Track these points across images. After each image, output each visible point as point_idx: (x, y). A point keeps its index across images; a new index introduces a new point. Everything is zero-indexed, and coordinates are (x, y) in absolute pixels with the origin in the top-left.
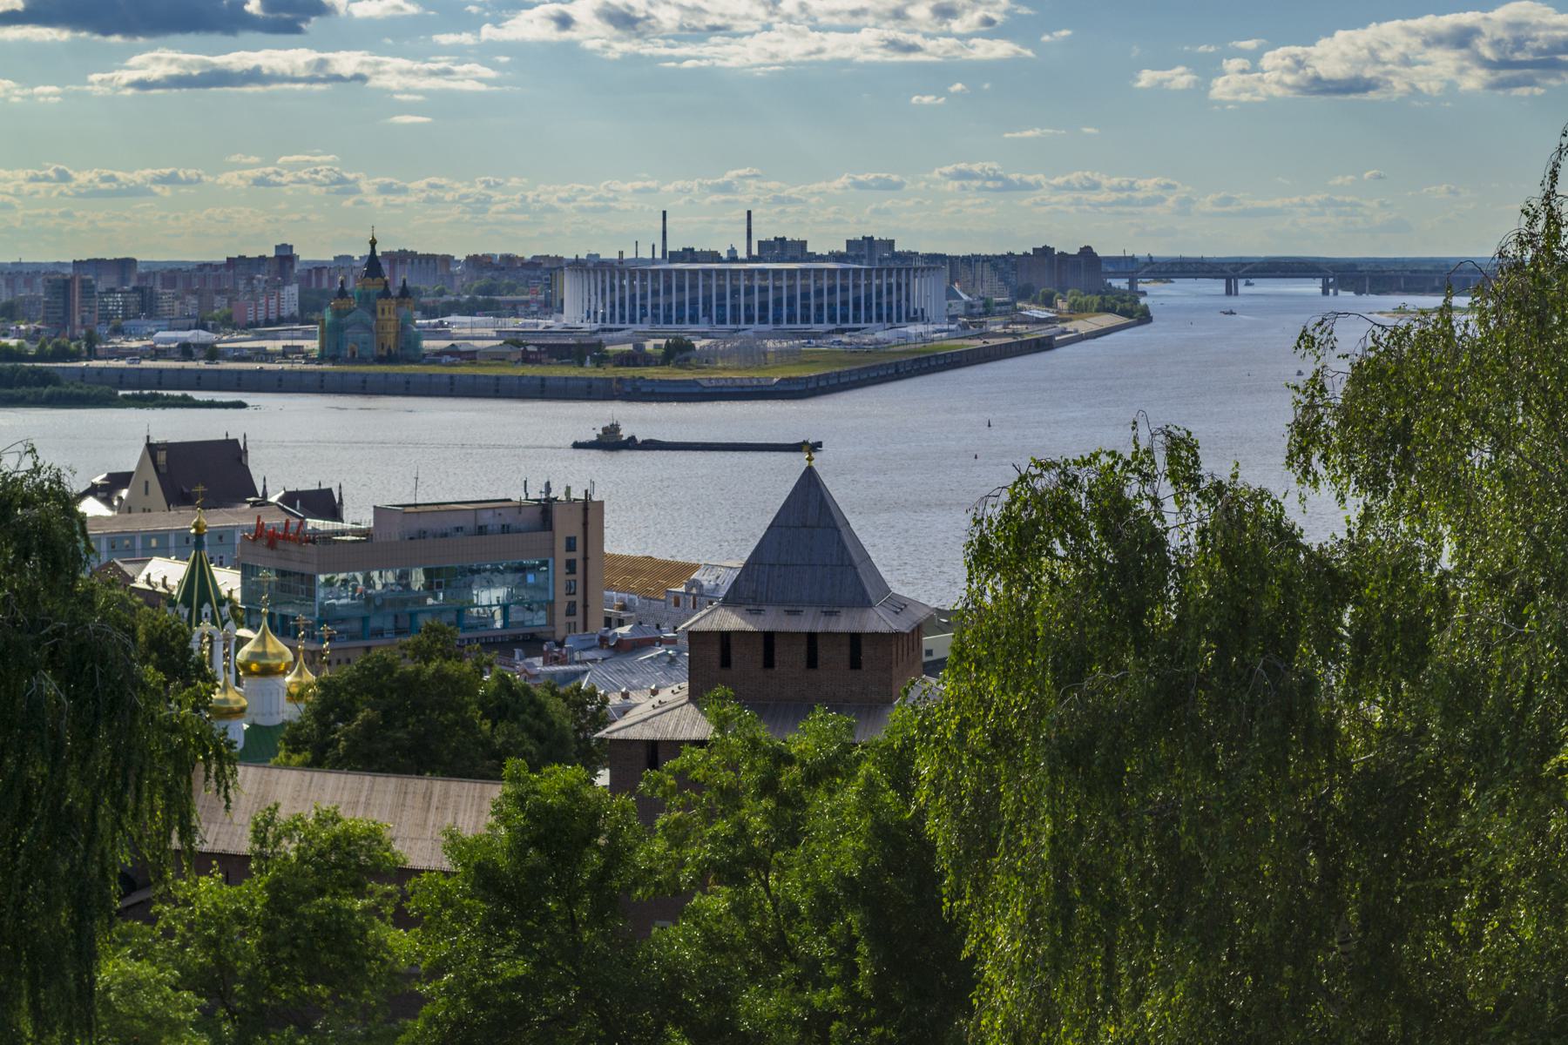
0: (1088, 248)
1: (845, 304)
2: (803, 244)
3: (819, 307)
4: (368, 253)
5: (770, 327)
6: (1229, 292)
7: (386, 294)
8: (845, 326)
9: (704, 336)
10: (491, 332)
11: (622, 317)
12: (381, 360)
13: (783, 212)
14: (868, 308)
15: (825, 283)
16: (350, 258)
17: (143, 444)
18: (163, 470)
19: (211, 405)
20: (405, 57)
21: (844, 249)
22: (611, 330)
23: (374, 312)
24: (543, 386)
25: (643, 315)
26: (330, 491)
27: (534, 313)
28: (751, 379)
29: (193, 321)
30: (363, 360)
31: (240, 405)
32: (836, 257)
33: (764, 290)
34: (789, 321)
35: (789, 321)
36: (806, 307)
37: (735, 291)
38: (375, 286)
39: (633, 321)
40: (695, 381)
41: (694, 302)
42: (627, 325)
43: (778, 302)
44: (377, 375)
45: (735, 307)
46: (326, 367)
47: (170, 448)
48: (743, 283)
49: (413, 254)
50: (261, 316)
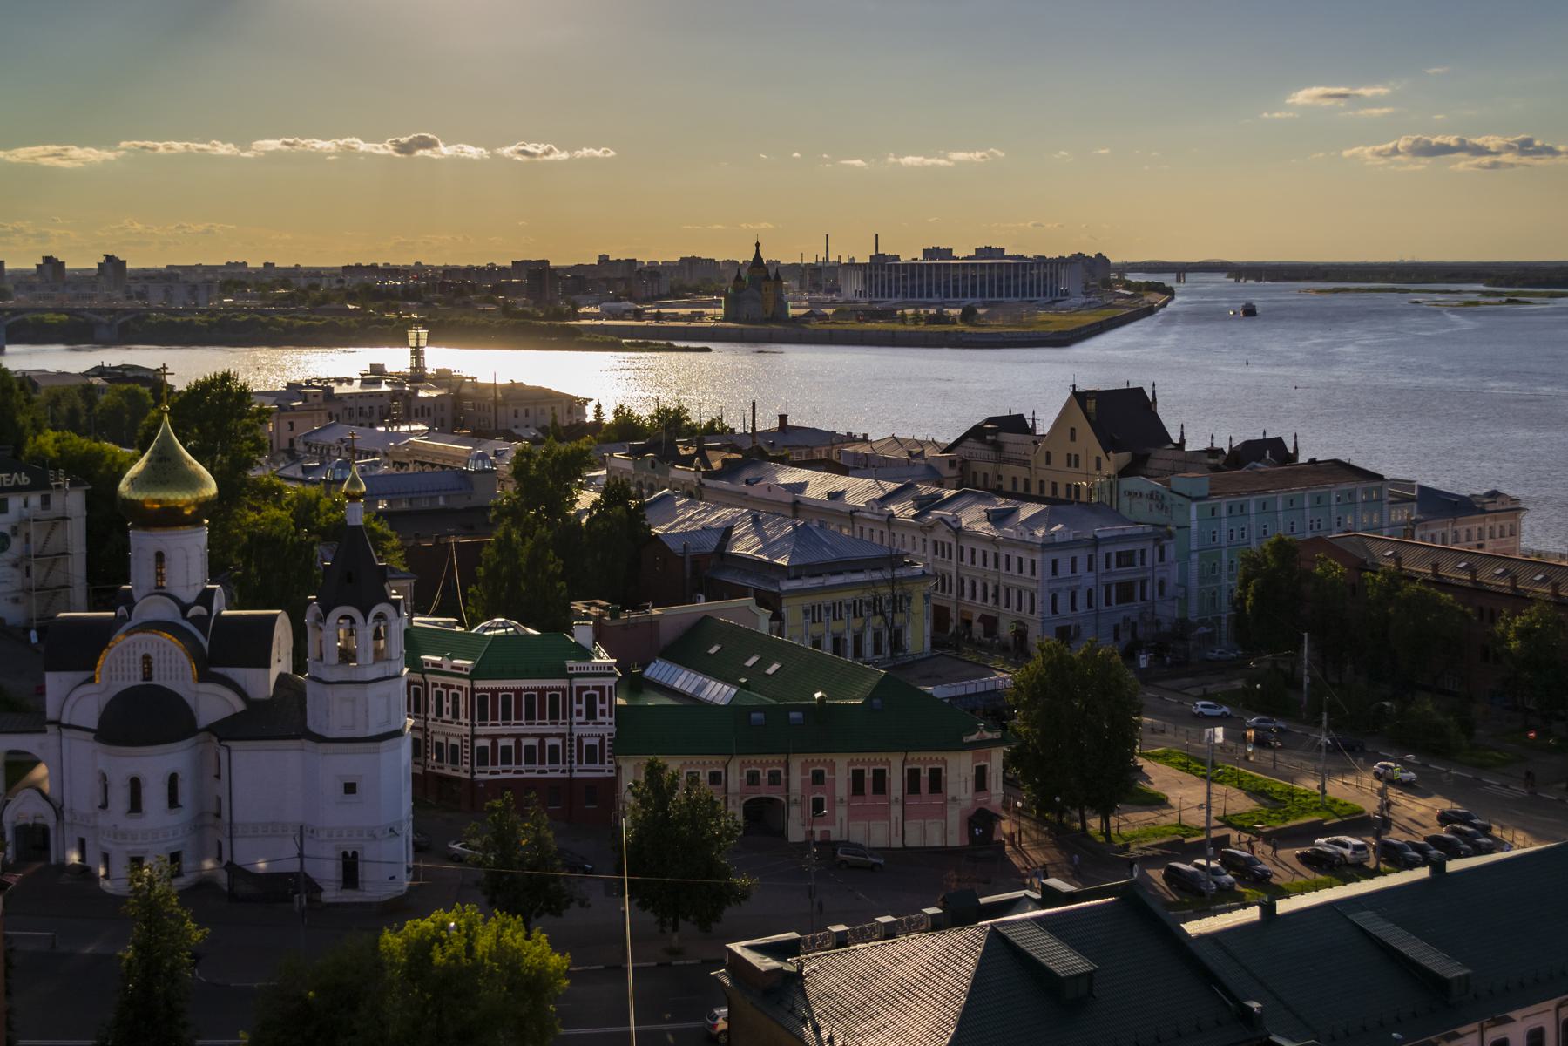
9: (984, 306)
14: (890, 288)
17: (1069, 393)
18: (1093, 418)
19: (687, 350)
25: (897, 292)
31: (708, 350)
32: (969, 258)
33: (974, 277)
36: (1000, 288)
39: (890, 296)
48: (969, 272)
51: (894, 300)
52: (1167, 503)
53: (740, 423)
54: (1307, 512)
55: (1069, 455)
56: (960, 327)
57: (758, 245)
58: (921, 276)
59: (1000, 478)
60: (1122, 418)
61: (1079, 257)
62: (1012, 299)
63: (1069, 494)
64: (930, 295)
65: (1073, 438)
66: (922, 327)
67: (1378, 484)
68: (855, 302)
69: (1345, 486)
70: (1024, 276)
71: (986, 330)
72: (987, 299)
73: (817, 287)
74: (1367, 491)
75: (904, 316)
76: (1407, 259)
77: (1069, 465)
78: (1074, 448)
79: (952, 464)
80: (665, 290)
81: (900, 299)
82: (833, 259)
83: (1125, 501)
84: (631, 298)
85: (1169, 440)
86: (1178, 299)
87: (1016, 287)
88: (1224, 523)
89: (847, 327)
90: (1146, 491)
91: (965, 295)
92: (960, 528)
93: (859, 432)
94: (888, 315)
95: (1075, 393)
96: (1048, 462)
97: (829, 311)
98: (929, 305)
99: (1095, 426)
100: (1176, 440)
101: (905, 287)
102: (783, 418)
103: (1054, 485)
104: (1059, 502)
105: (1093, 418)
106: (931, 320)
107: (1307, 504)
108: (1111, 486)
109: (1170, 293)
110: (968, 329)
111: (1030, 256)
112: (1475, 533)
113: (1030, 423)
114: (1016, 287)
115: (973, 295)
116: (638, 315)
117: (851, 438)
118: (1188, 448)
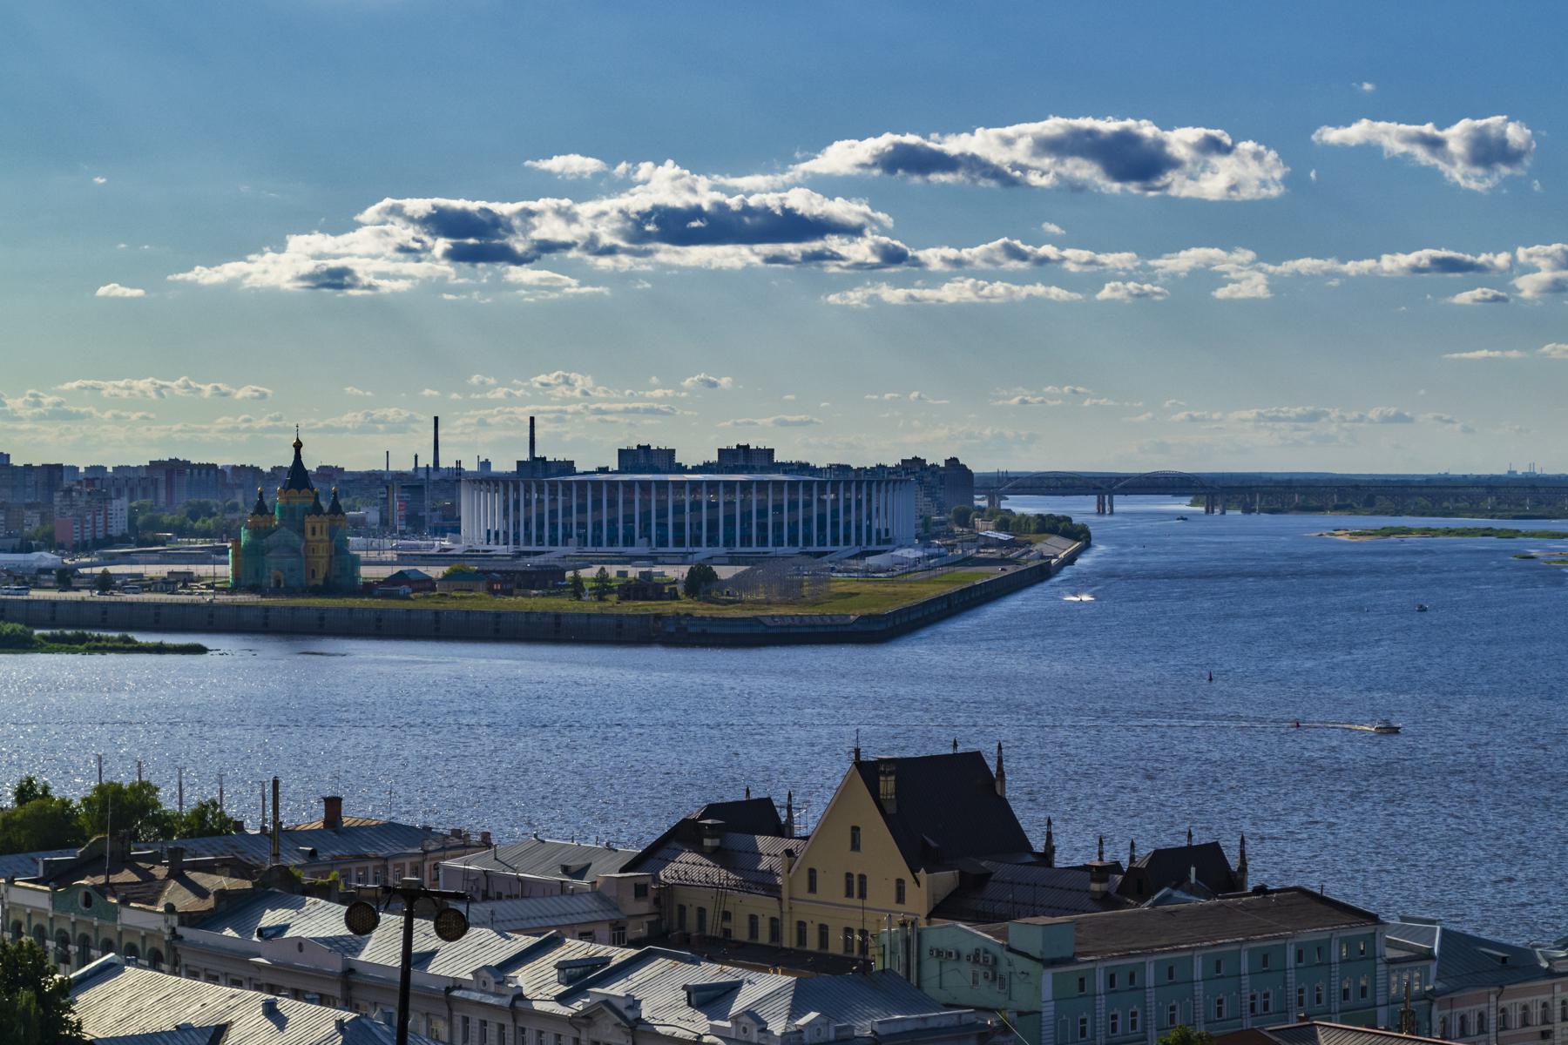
0: (955, 460)
1: (808, 521)
2: (671, 453)
3: (778, 526)
4: (288, 462)
5: (721, 550)
6: (1101, 512)
7: (317, 509)
8: (630, 550)
9: (733, 560)
10: (390, 555)
11: (540, 540)
12: (316, 592)
13: (482, 423)
15: (687, 498)
16: (103, 469)
19: (160, 649)
20: (553, 196)
21: (714, 458)
22: (528, 554)
23: (302, 531)
24: (558, 625)
26: (767, 802)
27: (402, 533)
28: (821, 616)
29: (17, 541)
30: (291, 592)
31: (200, 650)
32: (706, 468)
33: (713, 506)
34: (625, 544)
35: (727, 544)
36: (762, 527)
37: (679, 509)
38: (300, 500)
39: (553, 542)
40: (756, 618)
41: (629, 519)
42: (545, 548)
43: (730, 520)
44: (338, 610)
45: (679, 527)
46: (241, 598)
47: (902, 767)
48: (704, 498)
49: (187, 464)
50: (88, 535)
51: (560, 550)
52: (1003, 969)
53: (257, 816)
54: (1246, 981)
55: (849, 876)
56: (683, 606)
57: (298, 446)
58: (612, 504)
59: (727, 916)
60: (944, 809)
61: (914, 467)
62: (786, 549)
63: (848, 944)
64: (629, 540)
65: (855, 846)
66: (613, 605)
67: (1369, 930)
68: (487, 555)
69: (1309, 935)
70: (808, 505)
71: (732, 612)
72: (738, 549)
73: (416, 524)
74: (1350, 942)
75: (577, 581)
76: (1521, 469)
77: (849, 894)
78: (857, 864)
79: (641, 891)
80: (118, 526)
81: (572, 550)
82: (446, 462)
83: (931, 967)
84: (49, 543)
85: (1025, 845)
86: (1100, 548)
87: (793, 527)
88: (1101, 1002)
89: (468, 605)
90: (967, 948)
91: (696, 541)
92: (639, 1020)
93: (473, 824)
94: (548, 579)
95: (860, 765)
96: (812, 888)
97: (436, 572)
98: (631, 560)
99: (897, 825)
100: (1038, 845)
101: (582, 525)
102: (333, 805)
103: (823, 930)
104: (824, 969)
105: (891, 809)
106: (633, 591)
107: (1245, 968)
108: (907, 941)
109: (1081, 536)
110: (701, 609)
111: (821, 463)
112: (1536, 1012)
113: (783, 815)
114: (793, 527)
115: (712, 541)
116: (65, 579)
117: (460, 842)
118: (1060, 861)
